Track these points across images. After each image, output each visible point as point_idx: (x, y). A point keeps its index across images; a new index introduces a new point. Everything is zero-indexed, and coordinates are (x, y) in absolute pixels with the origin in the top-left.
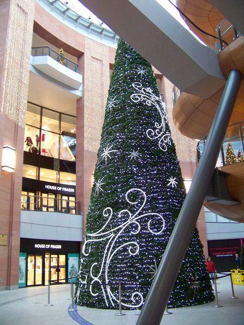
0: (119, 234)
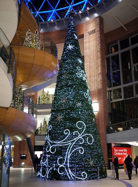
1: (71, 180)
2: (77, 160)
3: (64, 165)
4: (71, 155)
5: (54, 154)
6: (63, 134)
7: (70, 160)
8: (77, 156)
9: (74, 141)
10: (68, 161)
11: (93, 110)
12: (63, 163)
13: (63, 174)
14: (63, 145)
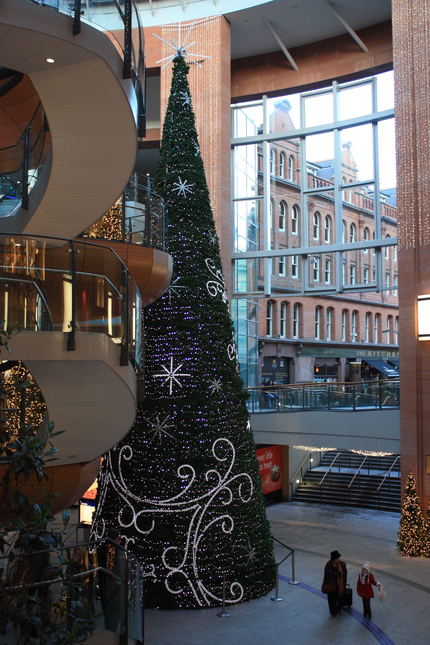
0: (206, 506)
1: (202, 608)
2: (219, 552)
3: (183, 568)
4: (202, 538)
5: (148, 537)
6: (172, 477)
7: (198, 554)
8: (217, 541)
9: (208, 498)
10: (194, 558)
11: (173, 69)
12: (181, 562)
13: (181, 594)
14: (177, 511)
